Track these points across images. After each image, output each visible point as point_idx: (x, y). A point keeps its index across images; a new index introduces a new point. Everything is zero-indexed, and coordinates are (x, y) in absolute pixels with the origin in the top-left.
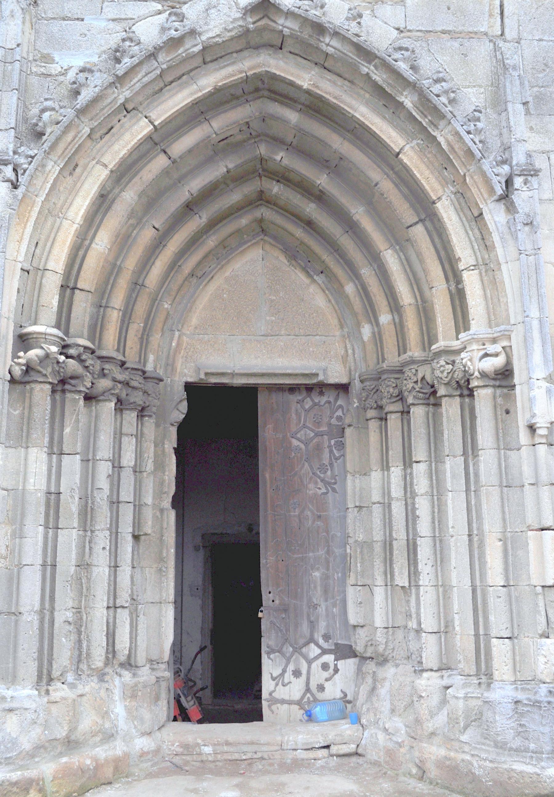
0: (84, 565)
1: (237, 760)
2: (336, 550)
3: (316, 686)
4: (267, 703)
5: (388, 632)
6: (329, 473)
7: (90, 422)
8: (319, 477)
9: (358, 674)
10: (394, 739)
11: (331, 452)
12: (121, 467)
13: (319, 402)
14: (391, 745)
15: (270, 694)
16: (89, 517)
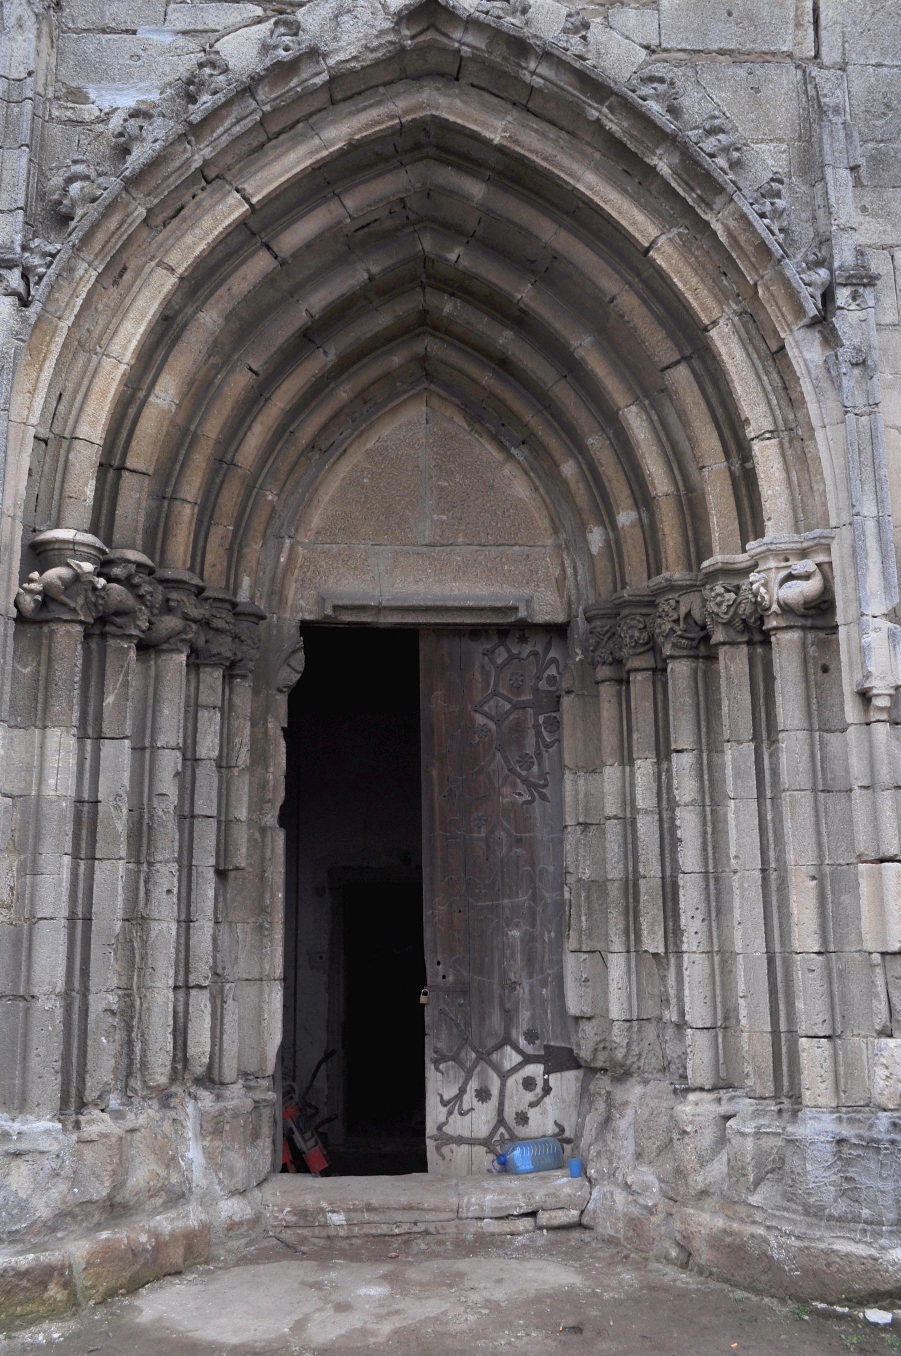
0: (136, 919)
1: (385, 1235)
2: (547, 895)
3: (514, 1116)
4: (435, 1143)
5: (630, 1027)
6: (535, 768)
7: (146, 686)
8: (519, 776)
9: (582, 1096)
10: (641, 1201)
11: (538, 734)
12: (196, 760)
13: (520, 653)
14: (635, 1211)
15: (440, 1128)
16: (145, 840)
